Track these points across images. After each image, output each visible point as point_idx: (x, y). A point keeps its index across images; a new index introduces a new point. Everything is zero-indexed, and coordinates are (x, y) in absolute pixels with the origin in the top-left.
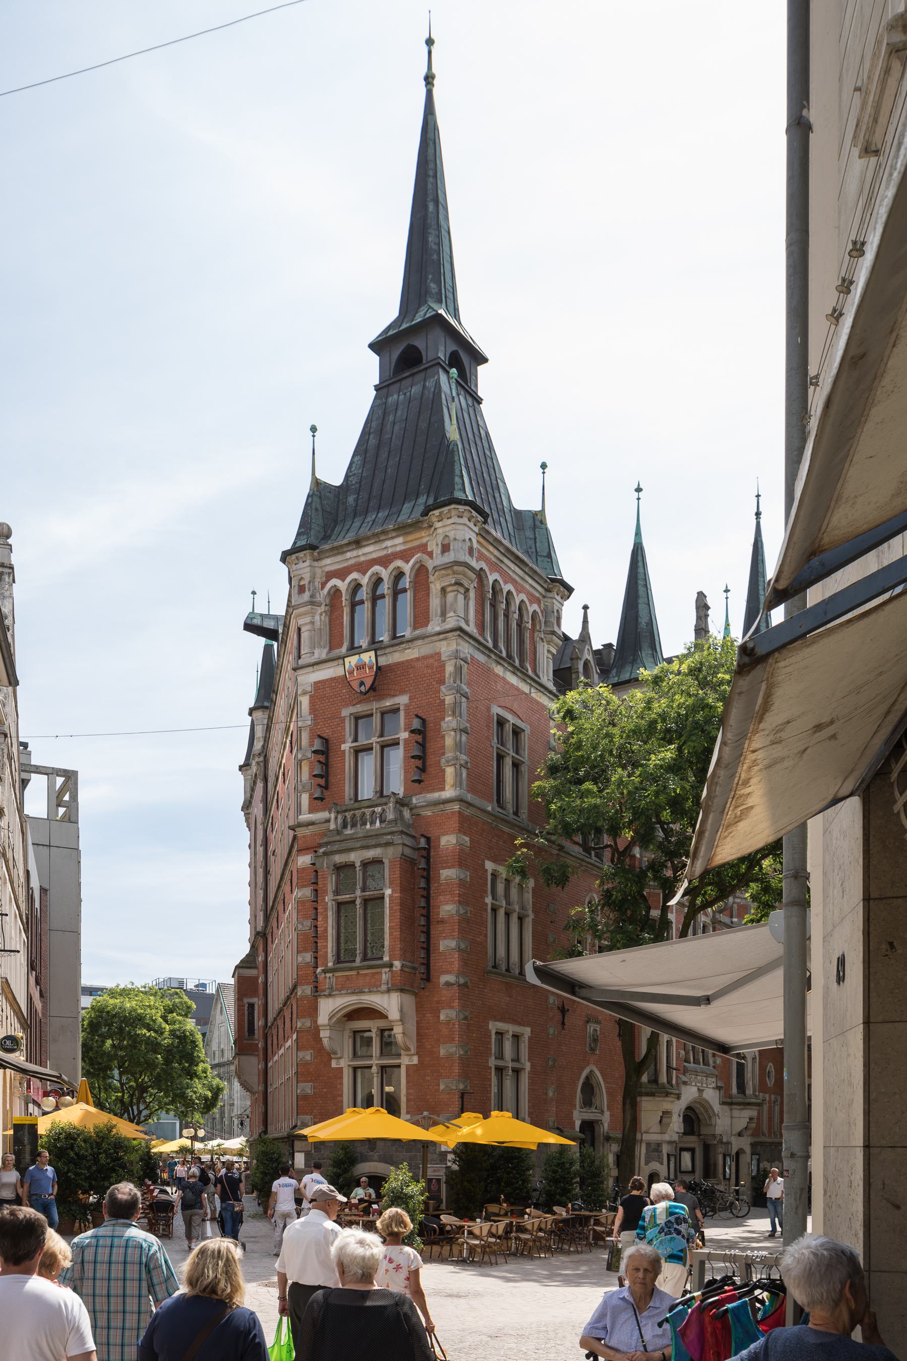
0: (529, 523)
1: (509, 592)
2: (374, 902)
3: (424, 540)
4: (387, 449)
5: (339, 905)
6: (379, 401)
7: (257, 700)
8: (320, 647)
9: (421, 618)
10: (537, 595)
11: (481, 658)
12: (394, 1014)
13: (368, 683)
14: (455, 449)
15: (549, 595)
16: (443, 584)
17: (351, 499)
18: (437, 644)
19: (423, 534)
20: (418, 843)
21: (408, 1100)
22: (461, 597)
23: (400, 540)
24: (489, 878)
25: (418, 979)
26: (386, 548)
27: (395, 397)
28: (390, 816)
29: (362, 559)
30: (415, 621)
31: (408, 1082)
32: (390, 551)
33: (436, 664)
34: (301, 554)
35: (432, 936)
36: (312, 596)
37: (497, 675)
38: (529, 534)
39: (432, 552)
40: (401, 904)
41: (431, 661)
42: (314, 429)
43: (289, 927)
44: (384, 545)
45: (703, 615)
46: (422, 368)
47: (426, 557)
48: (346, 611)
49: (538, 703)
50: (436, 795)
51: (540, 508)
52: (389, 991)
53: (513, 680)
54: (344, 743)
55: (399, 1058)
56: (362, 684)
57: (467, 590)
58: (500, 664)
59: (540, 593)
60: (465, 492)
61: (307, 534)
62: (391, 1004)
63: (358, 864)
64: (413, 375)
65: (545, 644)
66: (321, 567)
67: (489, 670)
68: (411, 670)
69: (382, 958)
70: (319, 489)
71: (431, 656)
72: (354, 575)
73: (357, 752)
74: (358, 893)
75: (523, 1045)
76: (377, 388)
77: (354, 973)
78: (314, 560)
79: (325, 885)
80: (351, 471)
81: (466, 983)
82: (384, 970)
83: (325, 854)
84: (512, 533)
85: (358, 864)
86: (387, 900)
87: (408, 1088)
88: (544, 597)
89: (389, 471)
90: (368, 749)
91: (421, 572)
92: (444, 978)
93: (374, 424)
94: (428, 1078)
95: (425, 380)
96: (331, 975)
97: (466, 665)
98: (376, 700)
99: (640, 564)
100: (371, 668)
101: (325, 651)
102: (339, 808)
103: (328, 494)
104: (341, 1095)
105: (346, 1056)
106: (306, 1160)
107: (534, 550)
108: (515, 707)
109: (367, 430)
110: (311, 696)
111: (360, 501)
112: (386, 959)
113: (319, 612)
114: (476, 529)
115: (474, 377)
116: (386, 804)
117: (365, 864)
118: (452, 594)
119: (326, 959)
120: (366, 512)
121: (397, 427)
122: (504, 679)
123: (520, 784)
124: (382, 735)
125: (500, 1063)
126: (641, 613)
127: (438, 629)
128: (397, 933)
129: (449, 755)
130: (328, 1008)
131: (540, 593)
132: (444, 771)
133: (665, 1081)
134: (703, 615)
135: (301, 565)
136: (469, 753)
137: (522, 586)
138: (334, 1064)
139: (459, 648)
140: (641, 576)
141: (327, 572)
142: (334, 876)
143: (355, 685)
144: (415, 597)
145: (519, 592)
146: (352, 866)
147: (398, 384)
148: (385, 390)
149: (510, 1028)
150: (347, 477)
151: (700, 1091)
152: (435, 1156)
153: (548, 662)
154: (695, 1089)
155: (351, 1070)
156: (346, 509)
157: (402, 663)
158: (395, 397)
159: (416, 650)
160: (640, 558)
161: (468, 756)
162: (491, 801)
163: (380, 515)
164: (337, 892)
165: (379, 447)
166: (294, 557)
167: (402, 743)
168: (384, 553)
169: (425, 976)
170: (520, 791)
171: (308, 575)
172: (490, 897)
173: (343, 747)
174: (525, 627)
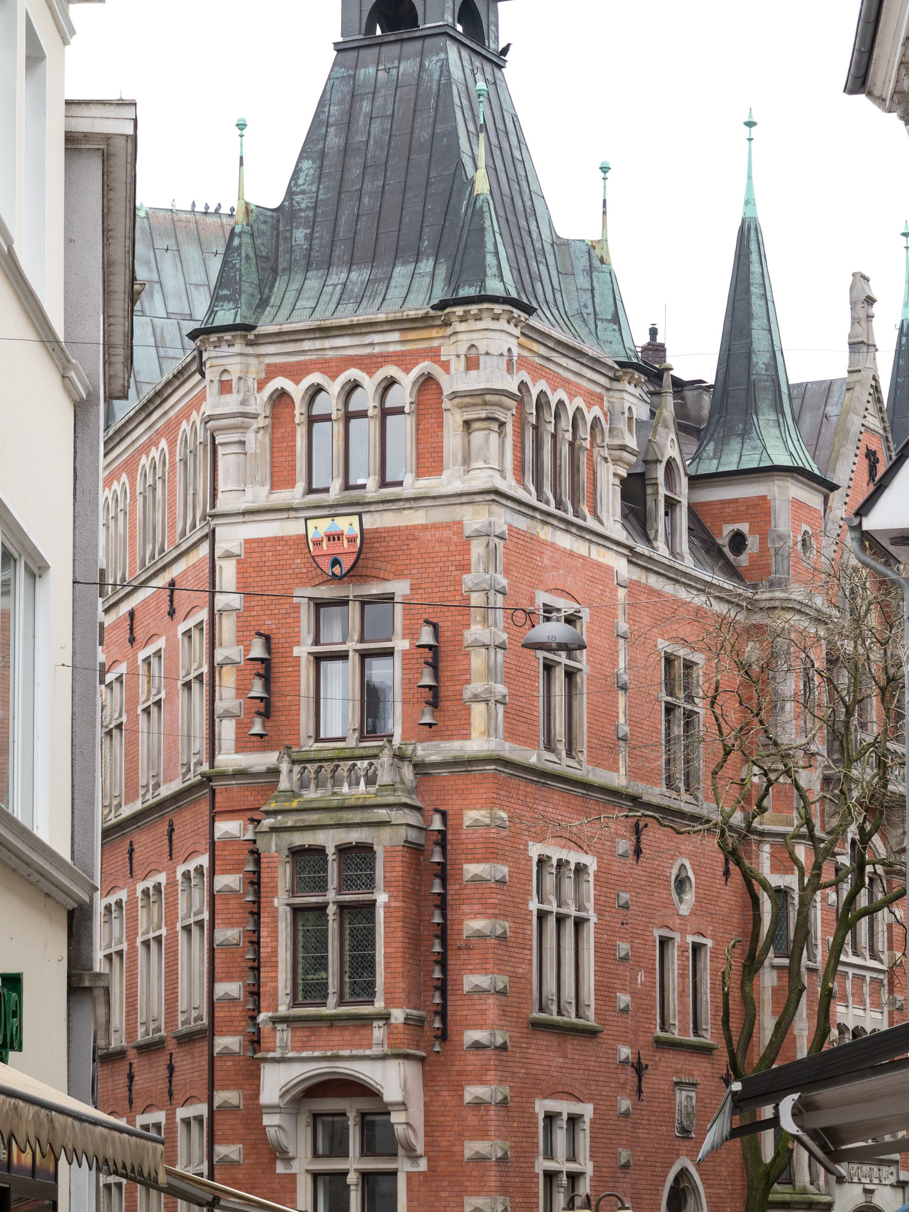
0: (582, 263)
1: (561, 403)
2: (359, 914)
3: (435, 343)
4: (359, 160)
5: (297, 911)
6: (341, 72)
8: (254, 482)
9: (429, 460)
10: (598, 390)
11: (522, 523)
12: (391, 1093)
13: (347, 562)
14: (485, 209)
15: (616, 385)
16: (467, 416)
17: (300, 234)
18: (457, 509)
19: (434, 333)
20: (430, 822)
22: (494, 437)
23: (396, 336)
24: (535, 869)
25: (431, 1040)
27: (372, 70)
28: (385, 777)
29: (330, 354)
30: (418, 464)
32: (377, 350)
35: (450, 967)
37: (544, 543)
38: (583, 281)
39: (448, 362)
40: (404, 919)
41: (447, 533)
44: (368, 339)
45: (862, 314)
46: (418, 34)
48: (301, 433)
49: (599, 565)
51: (598, 236)
52: (384, 1057)
53: (565, 541)
54: (298, 643)
55: (395, 1161)
56: (336, 562)
57: (502, 424)
58: (547, 523)
59: (603, 386)
60: (502, 280)
61: (236, 301)
62: (392, 1080)
63: (330, 850)
64: (402, 41)
65: (610, 464)
66: (258, 356)
67: (534, 538)
68: (413, 544)
71: (447, 526)
72: (315, 378)
73: (319, 659)
74: (331, 896)
75: (581, 1134)
76: (340, 49)
78: (247, 345)
79: (274, 879)
80: (296, 185)
81: (505, 1043)
82: (375, 1024)
83: (274, 830)
84: (557, 286)
88: (608, 389)
89: (366, 200)
92: (472, 1035)
94: (443, 1194)
95: (422, 55)
96: (284, 1026)
97: (502, 542)
98: (355, 584)
99: (754, 257)
100: (351, 540)
102: (295, 756)
103: (263, 226)
105: (301, 1154)
107: (591, 310)
108: (569, 585)
109: (323, 117)
110: (238, 562)
111: (316, 242)
112: (379, 1004)
113: (255, 426)
114: (517, 332)
115: (492, 28)
116: (376, 756)
117: (343, 850)
118: (482, 433)
119: (274, 995)
120: (328, 264)
121: (376, 127)
122: (552, 545)
123: (575, 704)
125: (551, 1165)
126: (756, 346)
128: (398, 966)
129: (477, 686)
130: (275, 1082)
131: (603, 386)
132: (469, 709)
133: (807, 1179)
134: (862, 314)
136: (508, 680)
137: (578, 386)
138: (280, 1168)
139: (493, 519)
140: (755, 278)
141: (268, 365)
142: (288, 868)
143: (325, 563)
144: (418, 425)
145: (572, 396)
146: (320, 851)
147: (375, 50)
148: (352, 55)
149: (565, 1107)
150: (290, 193)
151: (868, 1192)
153: (614, 491)
154: (858, 1189)
155: (309, 1179)
156: (291, 251)
157: (399, 529)
158: (372, 70)
159: (422, 513)
160: (753, 246)
161: (505, 683)
162: (534, 745)
163: (354, 275)
164: (293, 892)
165: (345, 151)
167: (398, 656)
169: (439, 1033)
170: (575, 715)
171: (238, 367)
172: (536, 899)
174: (581, 447)
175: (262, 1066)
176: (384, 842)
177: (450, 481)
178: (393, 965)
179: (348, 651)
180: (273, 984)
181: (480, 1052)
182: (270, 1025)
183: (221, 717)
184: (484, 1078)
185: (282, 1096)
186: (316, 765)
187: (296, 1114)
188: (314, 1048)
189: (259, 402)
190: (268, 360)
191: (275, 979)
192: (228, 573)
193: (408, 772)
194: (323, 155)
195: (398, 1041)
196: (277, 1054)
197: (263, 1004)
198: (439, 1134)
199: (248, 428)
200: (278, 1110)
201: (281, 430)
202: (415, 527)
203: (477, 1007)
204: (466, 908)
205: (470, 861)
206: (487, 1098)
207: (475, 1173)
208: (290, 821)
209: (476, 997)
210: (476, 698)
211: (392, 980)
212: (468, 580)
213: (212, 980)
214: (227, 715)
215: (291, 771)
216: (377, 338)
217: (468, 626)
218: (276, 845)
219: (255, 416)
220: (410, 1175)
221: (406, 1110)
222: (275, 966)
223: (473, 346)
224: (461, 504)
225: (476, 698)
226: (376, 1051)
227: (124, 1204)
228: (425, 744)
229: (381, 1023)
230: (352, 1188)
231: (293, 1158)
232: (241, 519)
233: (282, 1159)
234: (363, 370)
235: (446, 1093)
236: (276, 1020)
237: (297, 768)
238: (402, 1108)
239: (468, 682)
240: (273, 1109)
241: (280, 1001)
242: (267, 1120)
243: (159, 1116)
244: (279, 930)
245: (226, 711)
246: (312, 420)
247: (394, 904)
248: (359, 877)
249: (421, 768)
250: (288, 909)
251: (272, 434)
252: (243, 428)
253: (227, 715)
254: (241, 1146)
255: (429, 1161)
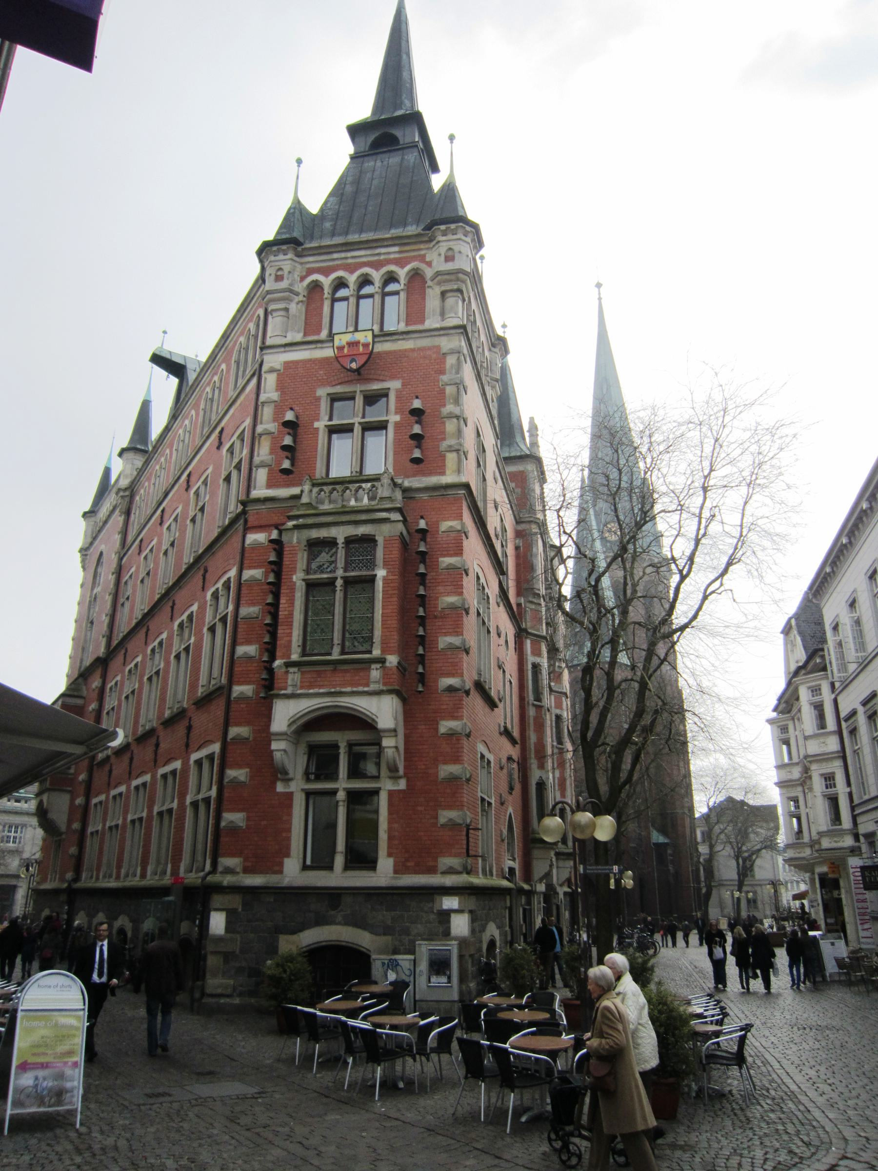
3: (422, 252)
5: (311, 586)
7: (132, 440)
16: (443, 288)
18: (436, 339)
21: (390, 838)
23: (396, 249)
26: (379, 254)
29: (350, 261)
31: (390, 813)
32: (382, 257)
33: (434, 356)
34: (284, 247)
36: (291, 285)
41: (428, 353)
42: (299, 162)
43: (538, 491)
47: (423, 266)
50: (433, 480)
54: (318, 420)
62: (385, 711)
63: (341, 541)
66: (302, 264)
69: (370, 652)
70: (297, 211)
71: (429, 348)
72: (340, 273)
77: (329, 668)
79: (295, 562)
82: (373, 666)
83: (296, 527)
85: (341, 541)
86: (379, 584)
87: (390, 822)
90: (347, 429)
91: (416, 276)
93: (350, 179)
94: (420, 808)
96: (295, 669)
101: (301, 334)
104: (289, 830)
106: (229, 923)
110: (278, 375)
112: (376, 652)
124: (363, 417)
127: (438, 326)
128: (394, 623)
130: (284, 714)
132: (444, 456)
135: (281, 257)
138: (280, 788)
144: (408, 298)
146: (331, 543)
152: (432, 916)
155: (303, 796)
157: (395, 352)
164: (308, 571)
166: (275, 248)
168: (376, 258)
173: (316, 425)
175: (274, 701)
176: (383, 533)
177: (432, 322)
178: (389, 622)
179: (353, 424)
180: (288, 638)
181: (453, 694)
182: (284, 669)
183: (258, 467)
184: (456, 714)
185: (289, 726)
186: (330, 487)
187: (296, 744)
188: (320, 687)
189: (301, 287)
190: (308, 266)
191: (290, 635)
192: (270, 381)
193: (398, 495)
194: (342, 194)
195: (392, 680)
196: (289, 691)
197: (278, 654)
198: (416, 759)
199: (291, 301)
200: (284, 737)
201: (314, 305)
202: (406, 350)
203: (450, 661)
204: (441, 589)
205: (445, 556)
206: (459, 729)
207: (448, 791)
208: (310, 521)
209: (449, 653)
210: (450, 449)
211: (388, 634)
212: (445, 378)
213: (234, 644)
214: (262, 465)
215: (311, 491)
216: (383, 250)
217: (445, 405)
218: (298, 538)
219: (297, 294)
220: (391, 793)
221: (396, 736)
222: (290, 625)
223: (450, 249)
224: (440, 335)
225: (450, 449)
226: (373, 687)
227: (141, 850)
228: (410, 479)
229: (378, 666)
230: (341, 803)
231: (291, 779)
232: (282, 349)
233: (283, 780)
234: (372, 268)
235: (423, 727)
236: (289, 665)
237: (316, 490)
238: (393, 734)
239: (444, 439)
240: (281, 735)
241: (293, 651)
242: (274, 746)
243: (177, 765)
244: (296, 598)
245: (262, 462)
246: (334, 300)
247: (391, 577)
248: (360, 561)
249: (405, 490)
250: (304, 583)
251: (308, 305)
252: (288, 300)
253: (262, 465)
254: (248, 770)
255: (408, 781)
